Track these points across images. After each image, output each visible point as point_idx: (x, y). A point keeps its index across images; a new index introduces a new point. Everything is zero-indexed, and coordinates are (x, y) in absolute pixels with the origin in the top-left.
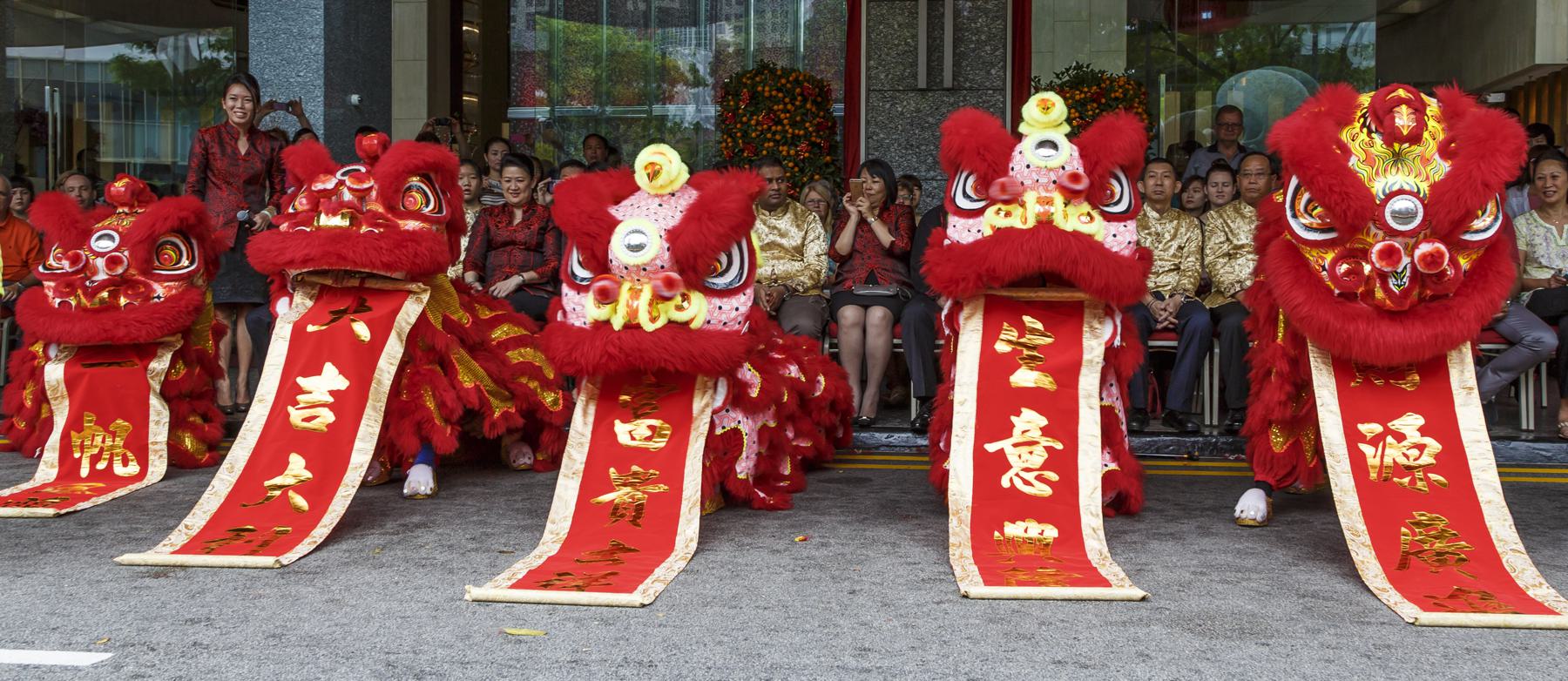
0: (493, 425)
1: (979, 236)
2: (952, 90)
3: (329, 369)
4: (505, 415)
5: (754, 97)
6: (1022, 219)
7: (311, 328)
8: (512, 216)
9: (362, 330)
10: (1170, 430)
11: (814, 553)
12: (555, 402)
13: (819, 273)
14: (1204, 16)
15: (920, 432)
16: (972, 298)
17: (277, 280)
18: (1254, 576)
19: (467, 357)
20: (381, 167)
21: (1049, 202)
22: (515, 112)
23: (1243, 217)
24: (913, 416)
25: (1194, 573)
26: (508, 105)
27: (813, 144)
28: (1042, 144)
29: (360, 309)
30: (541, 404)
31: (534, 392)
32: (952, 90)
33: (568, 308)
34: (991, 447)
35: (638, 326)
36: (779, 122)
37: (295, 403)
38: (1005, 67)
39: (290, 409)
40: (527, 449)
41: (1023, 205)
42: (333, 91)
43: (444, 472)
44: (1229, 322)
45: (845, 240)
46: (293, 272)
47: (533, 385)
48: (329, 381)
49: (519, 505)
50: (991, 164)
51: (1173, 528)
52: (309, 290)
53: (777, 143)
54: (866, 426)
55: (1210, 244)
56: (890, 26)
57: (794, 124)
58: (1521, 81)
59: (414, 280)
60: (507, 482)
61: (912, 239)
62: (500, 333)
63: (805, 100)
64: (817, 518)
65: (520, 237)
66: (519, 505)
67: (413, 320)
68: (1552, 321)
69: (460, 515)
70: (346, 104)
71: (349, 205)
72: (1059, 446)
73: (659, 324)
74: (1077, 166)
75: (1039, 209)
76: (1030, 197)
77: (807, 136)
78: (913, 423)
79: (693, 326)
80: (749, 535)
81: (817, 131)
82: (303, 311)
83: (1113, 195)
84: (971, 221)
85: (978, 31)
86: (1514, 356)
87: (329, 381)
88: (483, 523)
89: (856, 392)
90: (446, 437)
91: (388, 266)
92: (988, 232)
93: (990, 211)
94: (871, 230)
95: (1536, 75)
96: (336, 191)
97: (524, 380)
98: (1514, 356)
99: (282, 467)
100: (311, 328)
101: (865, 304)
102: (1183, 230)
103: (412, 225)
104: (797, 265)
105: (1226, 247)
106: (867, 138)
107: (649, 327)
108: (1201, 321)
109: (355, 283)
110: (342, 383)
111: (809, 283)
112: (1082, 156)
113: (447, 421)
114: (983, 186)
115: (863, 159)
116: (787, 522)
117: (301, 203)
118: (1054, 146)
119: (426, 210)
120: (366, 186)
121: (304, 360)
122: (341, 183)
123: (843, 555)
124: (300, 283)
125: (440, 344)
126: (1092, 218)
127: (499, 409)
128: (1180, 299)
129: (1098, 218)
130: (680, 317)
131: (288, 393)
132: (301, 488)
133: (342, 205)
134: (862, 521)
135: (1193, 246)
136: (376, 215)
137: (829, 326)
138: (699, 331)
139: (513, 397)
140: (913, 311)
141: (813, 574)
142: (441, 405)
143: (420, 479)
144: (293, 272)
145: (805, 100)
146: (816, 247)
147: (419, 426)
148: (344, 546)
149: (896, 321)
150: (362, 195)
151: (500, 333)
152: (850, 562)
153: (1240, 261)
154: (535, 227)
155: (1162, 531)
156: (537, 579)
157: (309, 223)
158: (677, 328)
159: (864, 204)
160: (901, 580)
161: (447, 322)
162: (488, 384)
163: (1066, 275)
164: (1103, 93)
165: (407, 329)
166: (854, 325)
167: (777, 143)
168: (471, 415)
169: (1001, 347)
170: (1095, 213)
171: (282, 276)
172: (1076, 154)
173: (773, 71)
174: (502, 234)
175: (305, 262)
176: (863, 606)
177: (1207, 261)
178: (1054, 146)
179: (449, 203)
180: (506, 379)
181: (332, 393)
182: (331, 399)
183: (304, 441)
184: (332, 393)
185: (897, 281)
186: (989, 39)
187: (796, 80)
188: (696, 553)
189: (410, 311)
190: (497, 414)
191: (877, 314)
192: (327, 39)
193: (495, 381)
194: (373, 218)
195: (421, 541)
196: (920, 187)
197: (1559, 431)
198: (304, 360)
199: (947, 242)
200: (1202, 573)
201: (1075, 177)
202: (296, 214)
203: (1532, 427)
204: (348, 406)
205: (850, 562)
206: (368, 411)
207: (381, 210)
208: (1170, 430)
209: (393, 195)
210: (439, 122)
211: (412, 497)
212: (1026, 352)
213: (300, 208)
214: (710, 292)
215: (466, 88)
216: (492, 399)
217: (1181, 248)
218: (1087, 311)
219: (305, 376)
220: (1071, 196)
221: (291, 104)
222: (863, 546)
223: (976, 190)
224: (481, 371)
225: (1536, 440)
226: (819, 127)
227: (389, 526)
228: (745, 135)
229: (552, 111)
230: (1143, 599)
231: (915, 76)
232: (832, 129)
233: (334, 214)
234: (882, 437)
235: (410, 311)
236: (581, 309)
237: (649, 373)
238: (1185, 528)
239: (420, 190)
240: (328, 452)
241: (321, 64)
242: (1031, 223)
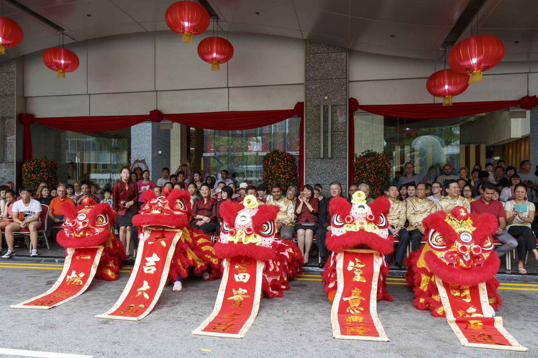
0: (197, 270)
1: (342, 234)
2: (331, 158)
3: (154, 255)
4: (201, 267)
5: (273, 161)
6: (354, 228)
7: (149, 243)
8: (204, 201)
9: (163, 243)
10: (397, 268)
11: (290, 318)
12: (216, 262)
13: (291, 219)
14: (407, 129)
15: (322, 267)
16: (340, 252)
17: (140, 228)
18: (422, 331)
19: (191, 251)
20: (169, 197)
21: (363, 224)
22: (205, 155)
23: (418, 202)
24: (320, 262)
25: (403, 329)
26: (203, 153)
27: (290, 174)
28: (360, 206)
29: (163, 237)
30: (211, 263)
31: (209, 259)
32: (331, 158)
33: (221, 239)
34: (345, 299)
35: (242, 242)
36: (280, 168)
37: (145, 265)
38: (346, 151)
39: (144, 267)
40: (208, 274)
41: (355, 224)
42: (154, 149)
43: (185, 282)
44: (415, 236)
45: (299, 210)
46: (144, 226)
47: (209, 257)
48: (154, 258)
49: (205, 295)
50: (345, 214)
51: (397, 308)
52: (148, 231)
53: (280, 174)
54: (306, 265)
55: (408, 210)
56: (312, 140)
57: (284, 169)
58: (507, 142)
59: (178, 228)
60: (202, 285)
61: (319, 209)
62: (200, 241)
63: (287, 162)
64: (290, 302)
65: (206, 207)
66: (205, 295)
67: (177, 240)
68: (516, 237)
69: (189, 299)
70: (157, 153)
71: (160, 207)
72: (364, 299)
73: (248, 243)
74: (370, 213)
75: (360, 226)
76: (357, 222)
77: (288, 171)
78: (320, 264)
79: (257, 244)
80: (271, 309)
81: (291, 170)
82: (147, 238)
83: (381, 221)
84: (339, 229)
85: (338, 141)
86: (504, 248)
87: (154, 258)
88: (195, 302)
89: (303, 253)
90: (184, 272)
91: (171, 225)
92: (345, 232)
93: (345, 226)
94: (306, 206)
95: (511, 141)
96: (157, 203)
97: (206, 256)
98: (504, 248)
99: (141, 285)
100: (149, 243)
101: (305, 228)
102: (400, 207)
103: (178, 213)
104: (285, 216)
105: (413, 211)
106: (306, 172)
107: (245, 243)
108: (406, 235)
109: (162, 229)
110: (158, 259)
111: (289, 222)
112: (372, 210)
113: (184, 268)
114: (343, 218)
115: (304, 184)
116: (282, 304)
117: (147, 207)
118: (364, 207)
119: (181, 209)
120: (165, 202)
121: (147, 253)
122: (159, 201)
123: (298, 318)
124: (146, 229)
125: (184, 248)
126: (375, 228)
127: (199, 265)
128: (399, 228)
129: (377, 228)
130: (254, 242)
131: (143, 262)
132: (147, 292)
133: (159, 207)
134: (304, 304)
135: (403, 211)
136: (168, 210)
137: (295, 235)
138: (259, 246)
139: (204, 261)
140: (319, 231)
141: (289, 326)
142: (183, 264)
143: (178, 286)
144: (144, 226)
145: (287, 162)
146: (291, 211)
147: (177, 270)
148: (156, 312)
149: (314, 234)
150: (164, 204)
151: (200, 241)
152: (300, 322)
153: (418, 216)
154: (210, 204)
155: (394, 310)
156: (212, 327)
157: (149, 212)
158: (252, 245)
159: (304, 199)
160: (315, 330)
161: (185, 240)
162: (196, 258)
163: (368, 245)
164: (376, 159)
165: (176, 243)
166: (302, 235)
167: (280, 174)
168: (191, 268)
169: (350, 268)
170: (376, 227)
171: (141, 227)
172: (370, 209)
173: (278, 153)
174: (201, 207)
175: (148, 223)
176: (304, 341)
177: (408, 215)
178: (364, 207)
179: (188, 207)
180: (201, 255)
181: (155, 262)
182: (155, 264)
183: (147, 277)
184: (155, 262)
185: (315, 222)
186: (342, 143)
187: (285, 156)
188: (257, 315)
189: (176, 238)
190: (199, 266)
191: (309, 232)
192: (152, 136)
193: (199, 257)
194: (167, 211)
195: (178, 310)
196: (321, 187)
197: (518, 271)
198: (147, 253)
199: (332, 235)
200: (406, 329)
201: (371, 217)
202: (145, 210)
203: (510, 269)
204: (160, 266)
205: (300, 322)
206: (165, 267)
207: (169, 209)
208: (397, 268)
209: (172, 204)
210: (183, 165)
211: (175, 291)
212: (357, 269)
213: (146, 208)
214: (262, 235)
215: (191, 145)
216: (197, 262)
217: (400, 212)
218: (374, 256)
219: (148, 257)
220: (369, 222)
221: (142, 160)
222: (304, 315)
223: (340, 220)
224: (194, 255)
225: (512, 274)
226: (292, 169)
227: (169, 303)
228: (270, 171)
229: (215, 154)
230: (388, 341)
231: (320, 154)
232: (296, 169)
233: (157, 210)
234: (310, 268)
235: (176, 238)
236: (225, 238)
237: (244, 257)
238: (401, 308)
239: (180, 203)
240: (154, 280)
241: (151, 143)
242: (358, 230)
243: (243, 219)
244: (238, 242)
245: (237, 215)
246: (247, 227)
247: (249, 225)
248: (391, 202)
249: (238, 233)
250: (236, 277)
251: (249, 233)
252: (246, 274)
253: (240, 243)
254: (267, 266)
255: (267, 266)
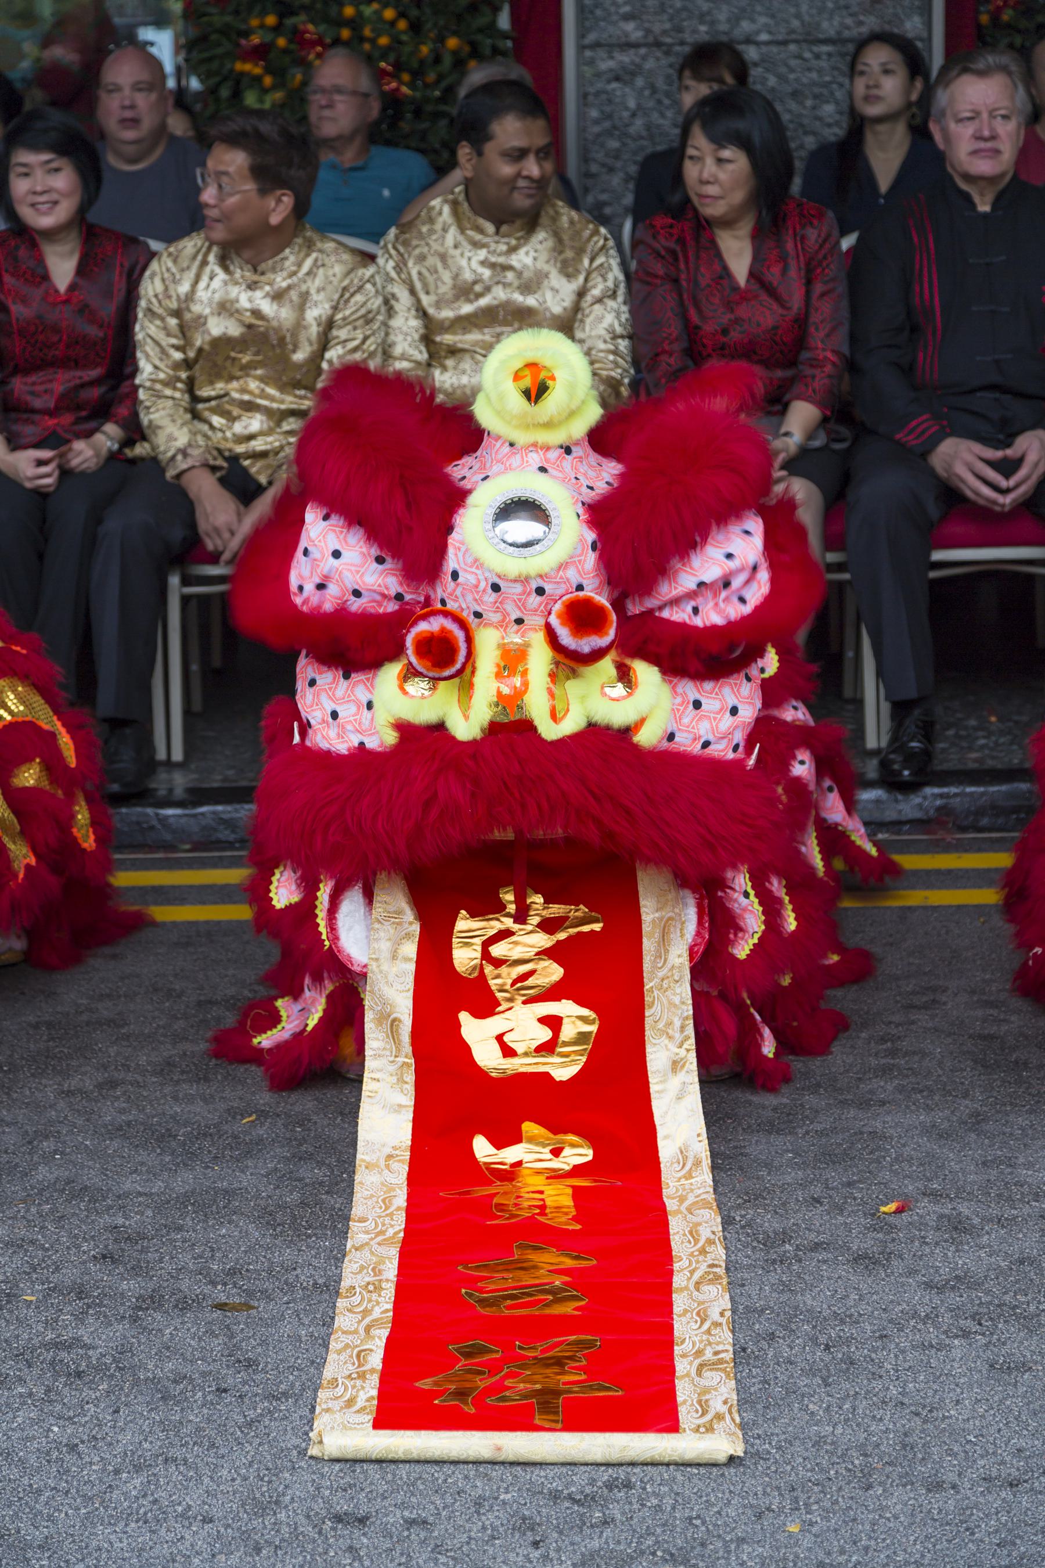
35: (527, 727)
73: (571, 725)
107: (550, 731)
158: (605, 742)
243: (521, 528)
244: (494, 728)
245: (457, 497)
246: (559, 591)
247: (573, 576)
248: (770, 438)
249: (488, 644)
250: (478, 1034)
251: (586, 644)
252: (566, 1008)
253: (511, 732)
254: (719, 922)
255: (719, 922)
